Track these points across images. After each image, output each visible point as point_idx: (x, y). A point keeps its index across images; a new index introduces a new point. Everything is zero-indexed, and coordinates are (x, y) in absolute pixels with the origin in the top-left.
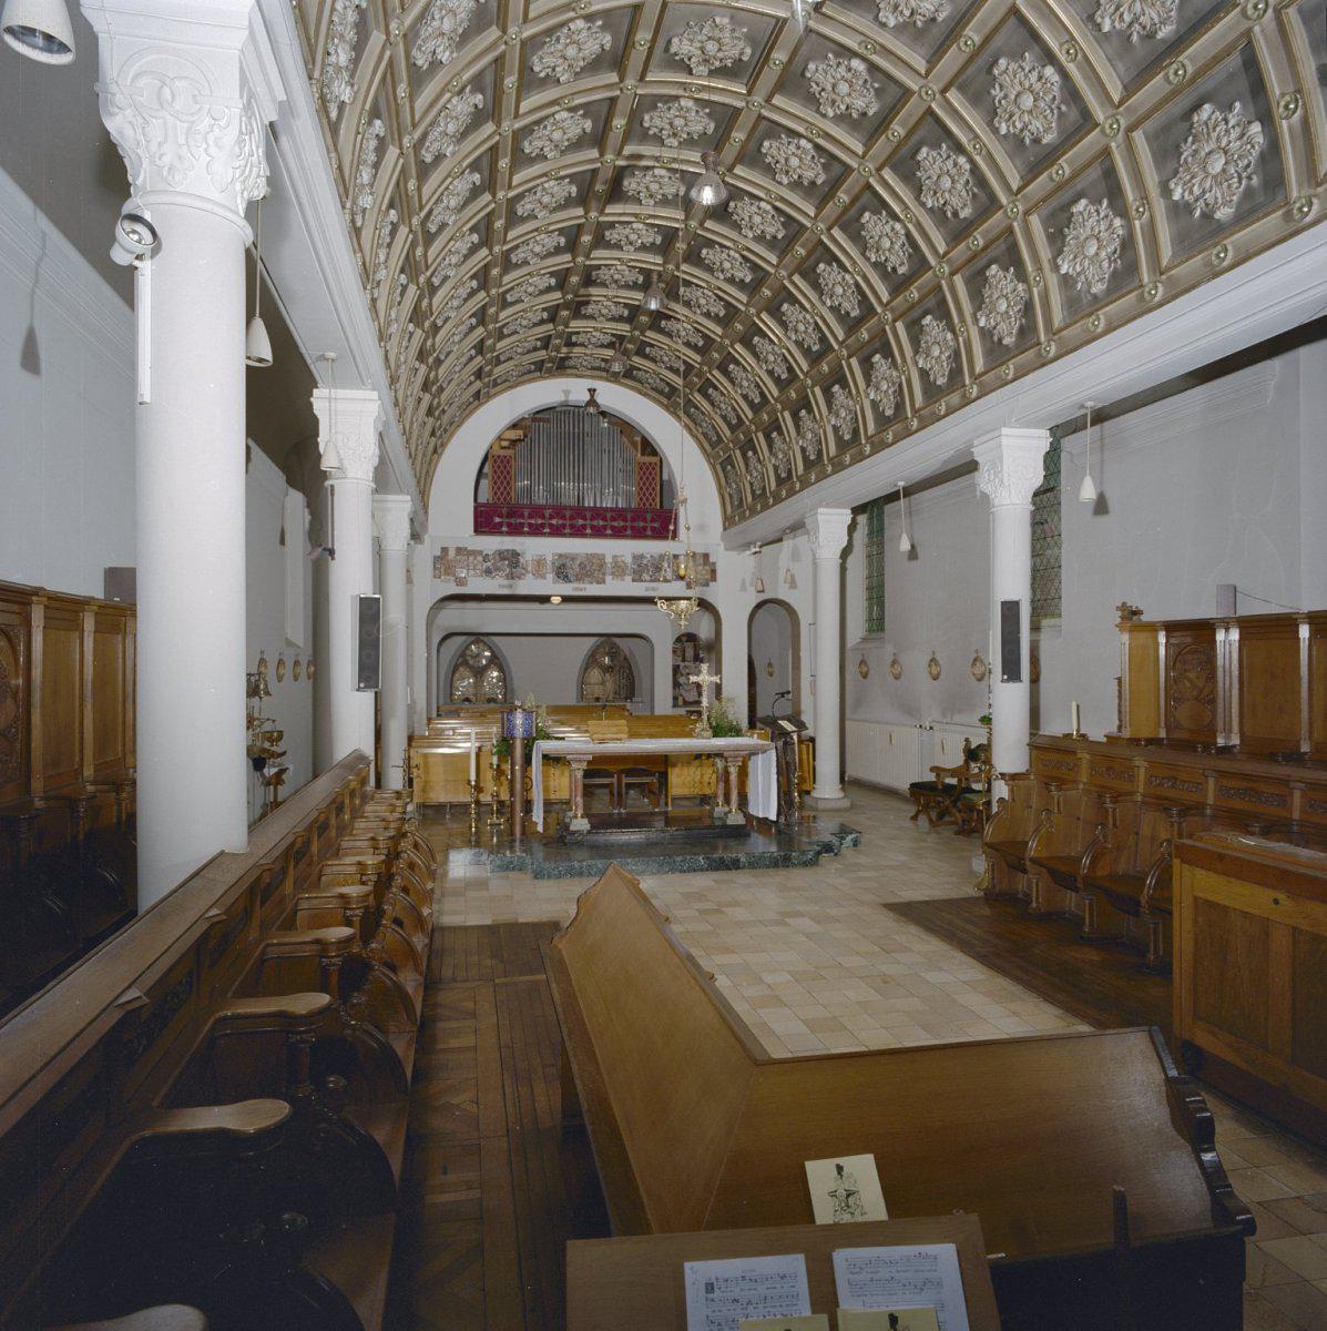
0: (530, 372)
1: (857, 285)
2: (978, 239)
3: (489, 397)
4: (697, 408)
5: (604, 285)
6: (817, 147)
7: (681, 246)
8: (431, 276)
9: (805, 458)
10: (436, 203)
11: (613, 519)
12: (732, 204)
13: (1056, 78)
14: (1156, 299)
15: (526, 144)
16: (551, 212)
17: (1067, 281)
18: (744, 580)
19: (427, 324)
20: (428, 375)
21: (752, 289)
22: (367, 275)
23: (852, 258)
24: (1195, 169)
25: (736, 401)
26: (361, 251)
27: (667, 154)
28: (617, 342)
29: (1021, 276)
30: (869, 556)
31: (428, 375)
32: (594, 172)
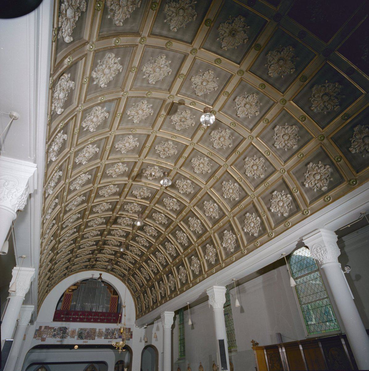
0: (83, 268)
1: (175, 248)
2: (204, 238)
3: (69, 275)
4: (131, 280)
5: (109, 245)
6: (166, 216)
7: (131, 236)
8: (60, 238)
9: (161, 296)
10: (67, 220)
11: (101, 316)
12: (144, 227)
13: (217, 206)
14: (258, 245)
15: (94, 209)
16: (97, 226)
17: (225, 249)
18: (141, 337)
19: (55, 252)
20: (51, 267)
21: (148, 248)
22: (42, 235)
23: (186, 229)
24: (248, 225)
25: (158, 265)
26: (43, 228)
27: (129, 214)
28: (110, 261)
29: (214, 247)
30: (180, 328)
31: (51, 267)
32: (110, 217)
